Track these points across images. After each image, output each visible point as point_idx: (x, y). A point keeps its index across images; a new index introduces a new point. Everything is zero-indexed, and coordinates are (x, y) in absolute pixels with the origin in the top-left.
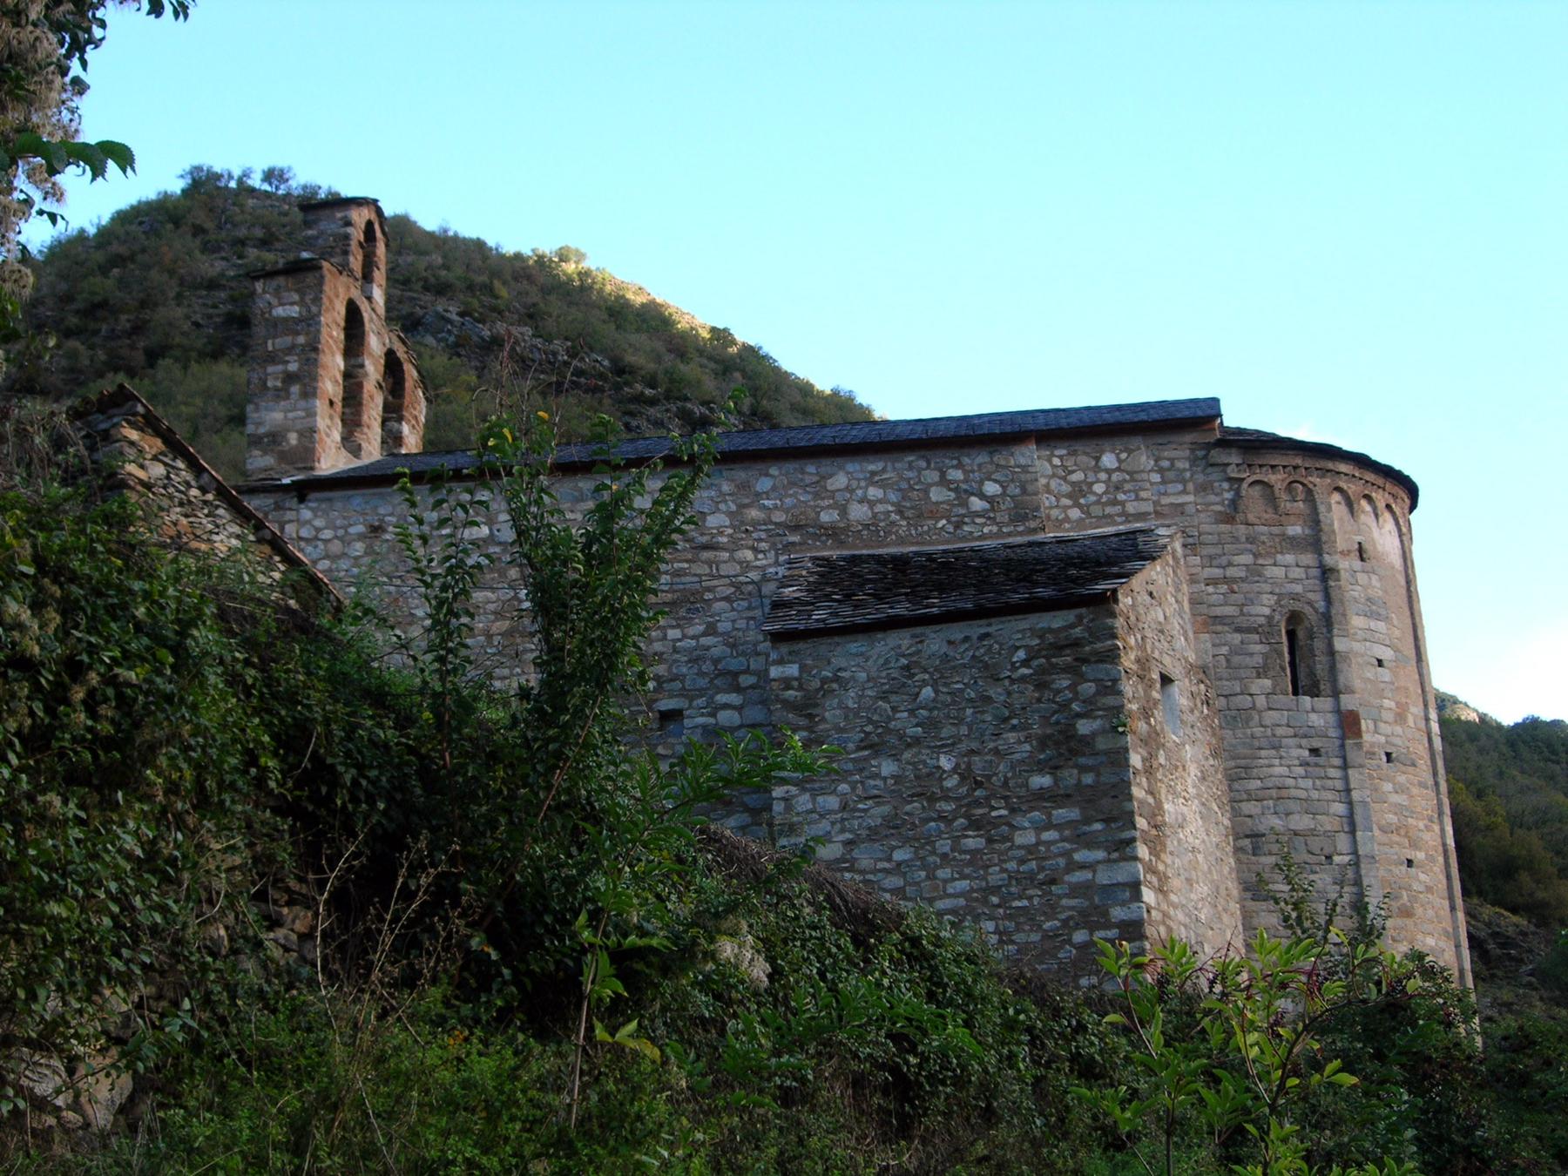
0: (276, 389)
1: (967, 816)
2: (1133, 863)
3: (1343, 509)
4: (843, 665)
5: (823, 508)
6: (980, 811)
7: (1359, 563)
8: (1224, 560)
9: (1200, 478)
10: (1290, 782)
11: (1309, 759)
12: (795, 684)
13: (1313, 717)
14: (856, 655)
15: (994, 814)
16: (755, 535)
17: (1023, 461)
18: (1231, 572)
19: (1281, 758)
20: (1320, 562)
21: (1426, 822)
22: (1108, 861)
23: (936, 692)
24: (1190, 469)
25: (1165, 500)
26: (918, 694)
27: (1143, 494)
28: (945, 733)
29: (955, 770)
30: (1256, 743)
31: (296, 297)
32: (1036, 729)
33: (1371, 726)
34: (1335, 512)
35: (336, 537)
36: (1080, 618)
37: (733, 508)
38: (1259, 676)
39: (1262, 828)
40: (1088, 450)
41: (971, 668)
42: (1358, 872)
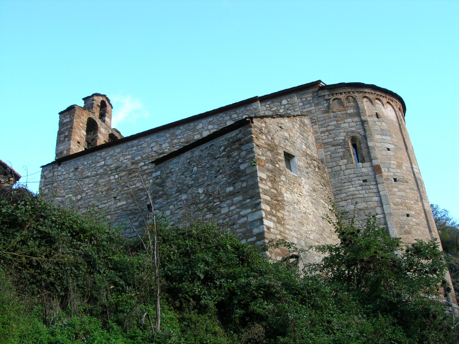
0: (62, 140)
1: (207, 207)
2: (260, 211)
3: (369, 103)
4: (172, 167)
5: (195, 135)
6: (211, 205)
7: (377, 119)
8: (326, 125)
9: (316, 101)
10: (357, 192)
11: (363, 184)
12: (159, 177)
13: (363, 169)
14: (176, 163)
15: (215, 204)
16: (176, 147)
17: (255, 107)
18: (329, 128)
19: (352, 185)
20: (361, 119)
21: (414, 201)
22: (252, 212)
23: (198, 168)
24: (313, 99)
25: (304, 110)
26: (193, 170)
27: (296, 109)
28: (200, 181)
29: (203, 193)
30: (343, 181)
31: (69, 116)
32: (228, 172)
33: (387, 170)
34: (365, 104)
35: (67, 173)
36: (240, 131)
37: (170, 141)
38: (342, 159)
39: (347, 210)
40: (277, 100)
41: (207, 157)
42: (385, 220)
